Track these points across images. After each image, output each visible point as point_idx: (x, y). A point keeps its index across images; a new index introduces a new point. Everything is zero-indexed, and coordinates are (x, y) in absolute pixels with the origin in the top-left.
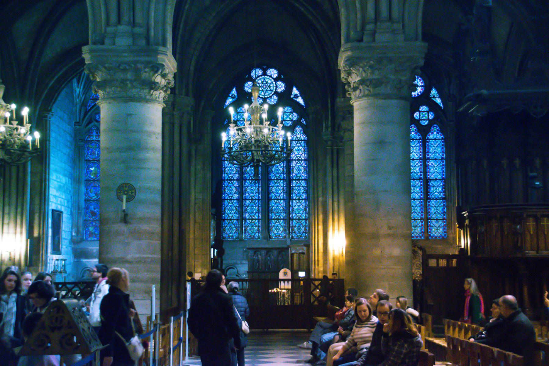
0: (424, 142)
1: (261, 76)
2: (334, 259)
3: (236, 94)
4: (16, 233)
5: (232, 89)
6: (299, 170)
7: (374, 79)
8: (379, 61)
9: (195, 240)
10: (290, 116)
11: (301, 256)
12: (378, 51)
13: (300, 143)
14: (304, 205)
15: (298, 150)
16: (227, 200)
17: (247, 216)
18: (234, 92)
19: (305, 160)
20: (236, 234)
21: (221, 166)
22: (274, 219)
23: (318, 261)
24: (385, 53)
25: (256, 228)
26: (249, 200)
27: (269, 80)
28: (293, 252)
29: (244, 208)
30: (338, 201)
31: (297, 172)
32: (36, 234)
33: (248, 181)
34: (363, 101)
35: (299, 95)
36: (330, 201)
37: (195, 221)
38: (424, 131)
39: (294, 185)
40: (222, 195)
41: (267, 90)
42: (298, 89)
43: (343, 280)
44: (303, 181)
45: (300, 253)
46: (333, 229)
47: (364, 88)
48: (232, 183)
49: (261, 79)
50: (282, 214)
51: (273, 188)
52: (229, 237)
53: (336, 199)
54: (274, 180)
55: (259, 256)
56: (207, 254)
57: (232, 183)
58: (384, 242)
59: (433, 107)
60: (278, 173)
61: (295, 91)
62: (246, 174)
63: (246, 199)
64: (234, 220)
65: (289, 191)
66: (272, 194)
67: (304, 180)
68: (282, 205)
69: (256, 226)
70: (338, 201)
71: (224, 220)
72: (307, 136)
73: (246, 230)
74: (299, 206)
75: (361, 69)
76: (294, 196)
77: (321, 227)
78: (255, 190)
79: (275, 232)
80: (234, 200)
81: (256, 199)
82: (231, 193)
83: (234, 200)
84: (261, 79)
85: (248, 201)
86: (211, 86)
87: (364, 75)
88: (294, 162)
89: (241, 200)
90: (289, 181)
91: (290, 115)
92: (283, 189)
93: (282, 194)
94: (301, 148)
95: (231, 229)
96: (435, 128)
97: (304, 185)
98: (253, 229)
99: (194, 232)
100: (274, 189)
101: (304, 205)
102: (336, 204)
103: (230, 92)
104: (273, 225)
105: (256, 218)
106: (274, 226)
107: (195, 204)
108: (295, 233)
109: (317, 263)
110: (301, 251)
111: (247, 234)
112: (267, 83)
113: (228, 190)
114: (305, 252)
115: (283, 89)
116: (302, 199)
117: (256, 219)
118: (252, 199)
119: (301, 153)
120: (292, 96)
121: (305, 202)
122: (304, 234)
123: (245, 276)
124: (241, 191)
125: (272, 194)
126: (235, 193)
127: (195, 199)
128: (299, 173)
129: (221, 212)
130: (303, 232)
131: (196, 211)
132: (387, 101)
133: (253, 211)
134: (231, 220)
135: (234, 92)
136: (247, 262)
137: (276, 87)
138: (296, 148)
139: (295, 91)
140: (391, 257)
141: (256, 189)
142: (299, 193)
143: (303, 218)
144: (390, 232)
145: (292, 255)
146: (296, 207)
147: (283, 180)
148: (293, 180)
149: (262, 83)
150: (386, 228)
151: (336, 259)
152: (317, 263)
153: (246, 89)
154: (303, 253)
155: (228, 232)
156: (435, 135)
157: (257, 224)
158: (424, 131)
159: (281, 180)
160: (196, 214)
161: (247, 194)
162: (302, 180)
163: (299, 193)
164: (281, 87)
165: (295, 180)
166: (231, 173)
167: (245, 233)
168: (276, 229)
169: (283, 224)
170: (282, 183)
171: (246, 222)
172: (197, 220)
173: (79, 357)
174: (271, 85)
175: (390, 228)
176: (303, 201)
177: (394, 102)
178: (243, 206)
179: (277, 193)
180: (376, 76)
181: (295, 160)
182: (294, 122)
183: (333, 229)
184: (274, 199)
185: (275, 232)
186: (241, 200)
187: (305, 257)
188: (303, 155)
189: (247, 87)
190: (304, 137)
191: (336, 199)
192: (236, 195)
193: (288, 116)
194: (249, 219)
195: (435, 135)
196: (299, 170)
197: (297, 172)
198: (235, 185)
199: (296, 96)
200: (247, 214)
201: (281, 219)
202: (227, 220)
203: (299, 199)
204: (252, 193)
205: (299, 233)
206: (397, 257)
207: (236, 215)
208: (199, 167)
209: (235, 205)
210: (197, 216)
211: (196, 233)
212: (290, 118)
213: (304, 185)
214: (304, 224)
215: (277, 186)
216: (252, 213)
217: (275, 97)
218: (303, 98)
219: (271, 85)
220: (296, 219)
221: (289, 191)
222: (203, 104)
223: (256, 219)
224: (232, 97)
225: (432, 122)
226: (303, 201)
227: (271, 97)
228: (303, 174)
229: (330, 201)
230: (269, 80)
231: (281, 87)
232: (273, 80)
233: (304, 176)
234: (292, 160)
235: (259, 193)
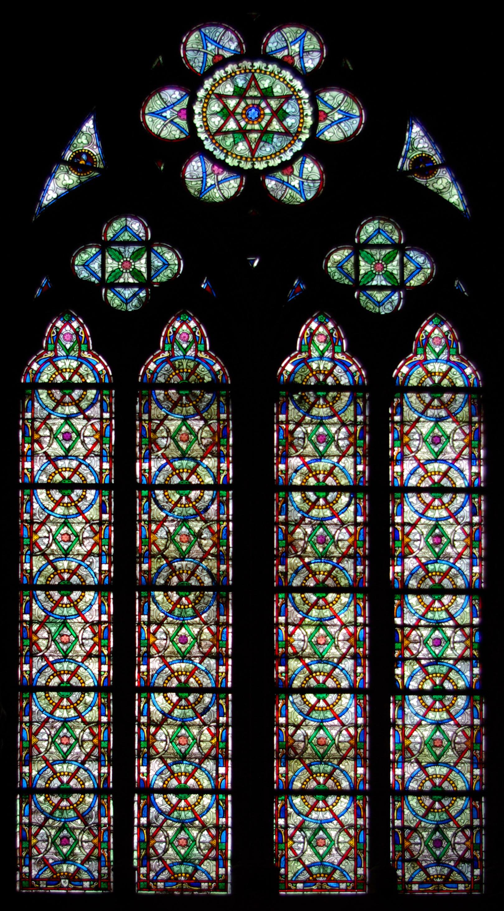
0: (379, 397)
1: (236, 59)
3: (96, 151)
5: (75, 129)
6: (438, 538)
10: (394, 267)
13: (444, 405)
14: (464, 719)
15: (436, 440)
16: (46, 689)
17: (153, 771)
18: (87, 139)
19: (469, 491)
20: (93, 865)
21: (14, 513)
22: (302, 792)
25: (205, 837)
26: (164, 690)
27: (276, 81)
29: (140, 734)
31: (426, 554)
33: (160, 596)
35: (437, 159)
38: (380, 343)
39: (410, 620)
40: (16, 665)
41: (264, 132)
42: (430, 132)
44: (461, 600)
48: (74, 604)
49: (231, 77)
50: (347, 765)
51: (299, 634)
52: (55, 880)
54: (303, 589)
57: (74, 604)
59: (422, 221)
60: (325, 557)
61: (418, 140)
62: (150, 556)
63: (150, 689)
64: (84, 791)
65: (382, 646)
66: (294, 664)
67: (469, 591)
68: (348, 718)
69: (204, 827)
71: (31, 791)
72: (479, 367)
73: (147, 843)
74: (438, 724)
76: (408, 674)
78: (197, 638)
79: (309, 857)
80: (85, 690)
81: (202, 690)
82: (65, 657)
83: (85, 690)
84: (231, 77)
85: (159, 698)
88: (412, 498)
89: (123, 691)
90: (380, 595)
91: (389, 259)
92: (353, 638)
93: (348, 664)
94: (448, 426)
95: (65, 841)
96: (184, 329)
97: (464, 617)
98: (190, 843)
100: (299, 637)
101: (464, 719)
103: (66, 143)
104: (294, 820)
105: (206, 784)
106: (300, 827)
108: (414, 860)
111: (155, 864)
112: (266, 94)
113: (51, 638)
115: (351, 127)
116: (456, 692)
117: (201, 792)
118: (183, 690)
119: (450, 454)
120: (404, 165)
121: (470, 705)
122: (466, 868)
124: (124, 645)
125: (294, 664)
126: (89, 655)
128: (438, 559)
130: (461, 859)
133: (185, 745)
134: (65, 792)
135: (87, 139)
137: (317, 116)
138: (425, 427)
139: (418, 140)
141: (206, 634)
142: (437, 660)
143: (461, 785)
146: (426, 732)
147: (351, 589)
148: (405, 591)
149: (240, 94)
153: (154, 125)
155: (51, 857)
156: (436, 356)
157: (210, 817)
158: (380, 343)
159: (339, 590)
161: (155, 664)
162: (455, 592)
163: (437, 660)
164: (342, 117)
165: (418, 592)
166: (66, 554)
167: (145, 860)
168: (312, 843)
169: (348, 818)
170: (344, 608)
171: (151, 803)
174: (289, 108)
176: (461, 701)
178: (132, 720)
179: (321, 660)
181: (418, 490)
182: (412, 295)
184: (302, 691)
185: (309, 857)
186: (123, 691)
188: (463, 464)
189: (158, 114)
190: (465, 375)
192: (93, 664)
193: (126, 266)
194: (164, 791)
195: (436, 356)
196: (438, 538)
197: (426, 554)
198: (92, 616)
199: (424, 166)
200: (156, 765)
201: (340, 793)
202: (48, 791)
203: (438, 692)
204: (185, 657)
205: (438, 862)
207: (92, 766)
209: (92, 715)
212: (136, 273)
213: (464, 617)
214: (464, 819)
215: (321, 623)
216: (183, 758)
217: (311, 169)
218: (458, 179)
219: (289, 108)
220: (418, 793)
221: (382, 646)
223: (201, 792)
224: (73, 165)
225: (420, 304)
226: (461, 701)
227: (286, 166)
228: (463, 564)
230: (277, 81)
231: (342, 117)
232: (298, 84)
233: (469, 571)
234: (405, 489)
235: (219, 658)
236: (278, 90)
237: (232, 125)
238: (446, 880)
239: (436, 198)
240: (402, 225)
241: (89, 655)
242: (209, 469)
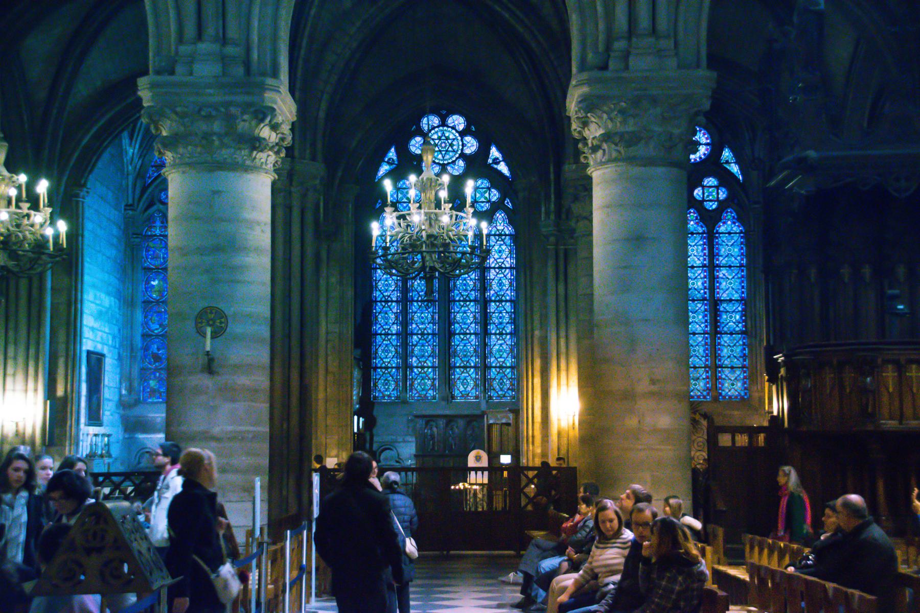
1: (438, 127)
2: (559, 434)
3: (395, 158)
4: (26, 391)
5: (389, 149)
6: (500, 284)
7: (627, 132)
8: (636, 102)
9: (326, 401)
10: (487, 195)
11: (505, 428)
12: (633, 85)
13: (503, 240)
14: (509, 343)
15: (500, 252)
16: (381, 334)
17: (414, 361)
18: (392, 154)
19: (510, 268)
20: (395, 392)
21: (370, 277)
22: (459, 367)
23: (533, 437)
24: (646, 90)
25: (429, 382)
26: (417, 334)
27: (452, 134)
28: (491, 422)
29: (409, 349)
30: (567, 337)
31: (497, 289)
32: (60, 392)
33: (415, 304)
34: (609, 170)
35: (501, 159)
36: (553, 337)
37: (327, 370)
39: (492, 310)
40: (371, 326)
41: (447, 151)
42: (499, 149)
43: (574, 469)
44: (508, 304)
45: (503, 424)
46: (559, 384)
47: (609, 148)
48: (389, 307)
49: (437, 132)
50: (473, 358)
51: (458, 316)
52: (383, 397)
53: (562, 333)
54: (459, 301)
55: (435, 430)
56: (347, 425)
57: (389, 307)
58: (643, 405)
60: (466, 290)
61: (494, 152)
62: (412, 291)
63: (412, 334)
64: (392, 368)
65: (484, 319)
66: (456, 325)
67: (510, 301)
68: (473, 343)
69: (429, 379)
70: (567, 337)
71: (376, 368)
72: (514, 227)
73: (412, 385)
74: (501, 345)
75: (605, 116)
76: (492, 328)
77: (537, 381)
78: (427, 317)
79: (462, 389)
80: (392, 334)
81: (428, 334)
82: (386, 324)
83: (392, 334)
84: (437, 132)
85: (415, 337)
86: (354, 143)
87: (610, 125)
88: (492, 271)
89: (404, 335)
90: (484, 303)
91: (485, 192)
92: (475, 317)
93: (473, 325)
94: (504, 247)
95: (386, 384)
97: (509, 309)
98: (425, 384)
99: (326, 389)
100: (459, 316)
101: (509, 343)
102: (562, 342)
103: (385, 154)
104: (457, 376)
105: (430, 364)
106: (459, 379)
107: (327, 341)
108: (494, 389)
109: (530, 440)
110: (504, 421)
111: (414, 392)
113: (382, 318)
114: (511, 422)
115: (474, 149)
116: (507, 334)
117: (428, 367)
118: (422, 334)
119: (504, 256)
120: (490, 161)
121: (511, 338)
122: (510, 392)
123: (410, 463)
124: (405, 319)
125: (456, 325)
126: (394, 323)
127: (327, 333)
128: (501, 290)
129: (370, 355)
130: (509, 389)
131: (329, 353)
132: (648, 168)
133: (424, 353)
134: (386, 368)
135: (392, 154)
136: (414, 439)
137: (463, 145)
138: (496, 248)
139: (494, 152)
140: (655, 430)
141: (430, 316)
142: (501, 323)
143: (508, 365)
144: (654, 388)
145: (490, 426)
146: (497, 347)
147: (474, 301)
148: (491, 301)
149: (440, 139)
150: (647, 381)
151: (563, 433)
152: (530, 440)
153: (413, 149)
154: (508, 424)
155: (382, 389)
156: (728, 226)
157: (431, 376)
159: (470, 301)
160: (329, 358)
161: (414, 326)
162: (506, 301)
163: (501, 323)
164: (471, 145)
165: (495, 301)
166: (387, 291)
167: (411, 390)
168: (463, 384)
169: (473, 376)
170: (472, 307)
171: (413, 371)
172: (330, 369)
173: (132, 598)
174: (455, 143)
175: (653, 382)
176: (508, 337)
177: (661, 170)
178: (407, 344)
179: (465, 324)
180: (631, 127)
181: (494, 268)
182: (493, 204)
183: (559, 384)
184: (459, 334)
185: (462, 389)
186: (404, 335)
187: (511, 430)
188: (508, 259)
189: (414, 146)
190: (509, 230)
191: (562, 333)
192: (395, 326)
194: (417, 367)
195: (728, 226)
196: (500, 284)
197: (497, 289)
198: (395, 310)
199: (496, 161)
200: (414, 359)
201: (471, 367)
202: (381, 368)
203: (501, 334)
204: (422, 323)
205: (501, 390)
206: (665, 430)
207: (395, 359)
208: (333, 280)
209: (394, 343)
210: (330, 362)
211: (328, 390)
213: (509, 309)
214: (509, 376)
215: (465, 312)
216: (423, 356)
217: (461, 163)
218: (508, 165)
219: (455, 143)
220: (495, 367)
221: (484, 319)
222: (340, 174)
223: (428, 367)
224: (388, 163)
226: (508, 337)
227: (454, 162)
228: (509, 292)
229: (553, 337)
230: (452, 134)
232: (457, 135)
233: (509, 294)
234: (490, 268)
235: (434, 324)
236: (451, 137)
237: (437, 141)
238: (504, 396)
239: (500, 173)
240: (491, 182)
241: (394, 323)
242: (430, 328)
